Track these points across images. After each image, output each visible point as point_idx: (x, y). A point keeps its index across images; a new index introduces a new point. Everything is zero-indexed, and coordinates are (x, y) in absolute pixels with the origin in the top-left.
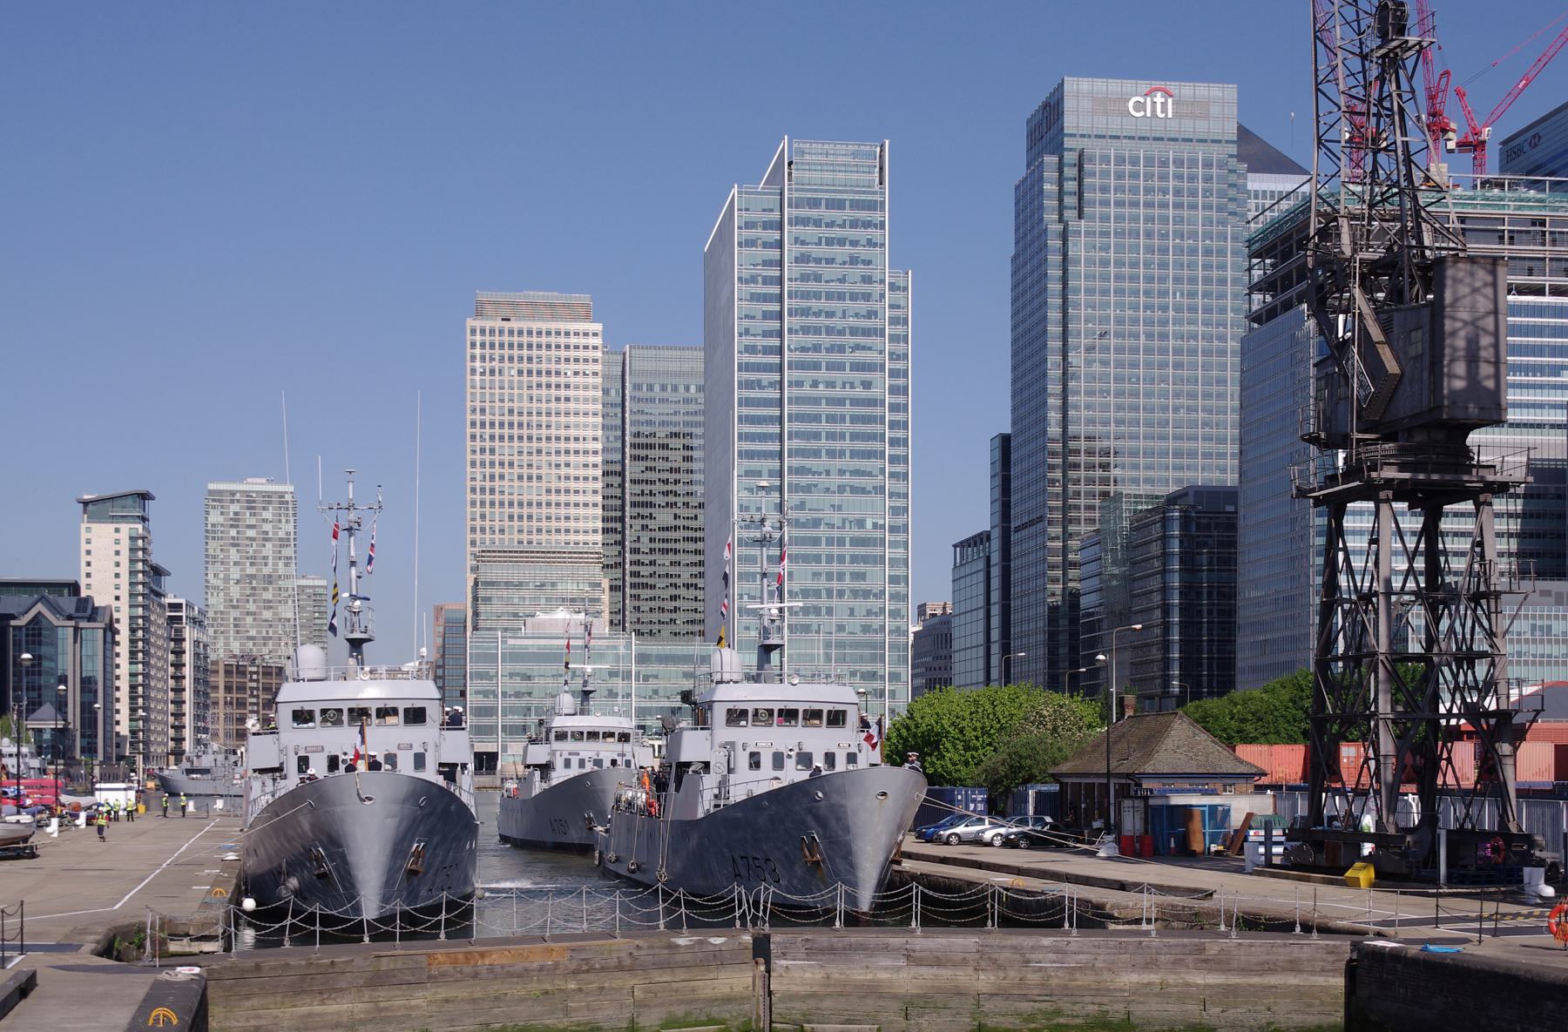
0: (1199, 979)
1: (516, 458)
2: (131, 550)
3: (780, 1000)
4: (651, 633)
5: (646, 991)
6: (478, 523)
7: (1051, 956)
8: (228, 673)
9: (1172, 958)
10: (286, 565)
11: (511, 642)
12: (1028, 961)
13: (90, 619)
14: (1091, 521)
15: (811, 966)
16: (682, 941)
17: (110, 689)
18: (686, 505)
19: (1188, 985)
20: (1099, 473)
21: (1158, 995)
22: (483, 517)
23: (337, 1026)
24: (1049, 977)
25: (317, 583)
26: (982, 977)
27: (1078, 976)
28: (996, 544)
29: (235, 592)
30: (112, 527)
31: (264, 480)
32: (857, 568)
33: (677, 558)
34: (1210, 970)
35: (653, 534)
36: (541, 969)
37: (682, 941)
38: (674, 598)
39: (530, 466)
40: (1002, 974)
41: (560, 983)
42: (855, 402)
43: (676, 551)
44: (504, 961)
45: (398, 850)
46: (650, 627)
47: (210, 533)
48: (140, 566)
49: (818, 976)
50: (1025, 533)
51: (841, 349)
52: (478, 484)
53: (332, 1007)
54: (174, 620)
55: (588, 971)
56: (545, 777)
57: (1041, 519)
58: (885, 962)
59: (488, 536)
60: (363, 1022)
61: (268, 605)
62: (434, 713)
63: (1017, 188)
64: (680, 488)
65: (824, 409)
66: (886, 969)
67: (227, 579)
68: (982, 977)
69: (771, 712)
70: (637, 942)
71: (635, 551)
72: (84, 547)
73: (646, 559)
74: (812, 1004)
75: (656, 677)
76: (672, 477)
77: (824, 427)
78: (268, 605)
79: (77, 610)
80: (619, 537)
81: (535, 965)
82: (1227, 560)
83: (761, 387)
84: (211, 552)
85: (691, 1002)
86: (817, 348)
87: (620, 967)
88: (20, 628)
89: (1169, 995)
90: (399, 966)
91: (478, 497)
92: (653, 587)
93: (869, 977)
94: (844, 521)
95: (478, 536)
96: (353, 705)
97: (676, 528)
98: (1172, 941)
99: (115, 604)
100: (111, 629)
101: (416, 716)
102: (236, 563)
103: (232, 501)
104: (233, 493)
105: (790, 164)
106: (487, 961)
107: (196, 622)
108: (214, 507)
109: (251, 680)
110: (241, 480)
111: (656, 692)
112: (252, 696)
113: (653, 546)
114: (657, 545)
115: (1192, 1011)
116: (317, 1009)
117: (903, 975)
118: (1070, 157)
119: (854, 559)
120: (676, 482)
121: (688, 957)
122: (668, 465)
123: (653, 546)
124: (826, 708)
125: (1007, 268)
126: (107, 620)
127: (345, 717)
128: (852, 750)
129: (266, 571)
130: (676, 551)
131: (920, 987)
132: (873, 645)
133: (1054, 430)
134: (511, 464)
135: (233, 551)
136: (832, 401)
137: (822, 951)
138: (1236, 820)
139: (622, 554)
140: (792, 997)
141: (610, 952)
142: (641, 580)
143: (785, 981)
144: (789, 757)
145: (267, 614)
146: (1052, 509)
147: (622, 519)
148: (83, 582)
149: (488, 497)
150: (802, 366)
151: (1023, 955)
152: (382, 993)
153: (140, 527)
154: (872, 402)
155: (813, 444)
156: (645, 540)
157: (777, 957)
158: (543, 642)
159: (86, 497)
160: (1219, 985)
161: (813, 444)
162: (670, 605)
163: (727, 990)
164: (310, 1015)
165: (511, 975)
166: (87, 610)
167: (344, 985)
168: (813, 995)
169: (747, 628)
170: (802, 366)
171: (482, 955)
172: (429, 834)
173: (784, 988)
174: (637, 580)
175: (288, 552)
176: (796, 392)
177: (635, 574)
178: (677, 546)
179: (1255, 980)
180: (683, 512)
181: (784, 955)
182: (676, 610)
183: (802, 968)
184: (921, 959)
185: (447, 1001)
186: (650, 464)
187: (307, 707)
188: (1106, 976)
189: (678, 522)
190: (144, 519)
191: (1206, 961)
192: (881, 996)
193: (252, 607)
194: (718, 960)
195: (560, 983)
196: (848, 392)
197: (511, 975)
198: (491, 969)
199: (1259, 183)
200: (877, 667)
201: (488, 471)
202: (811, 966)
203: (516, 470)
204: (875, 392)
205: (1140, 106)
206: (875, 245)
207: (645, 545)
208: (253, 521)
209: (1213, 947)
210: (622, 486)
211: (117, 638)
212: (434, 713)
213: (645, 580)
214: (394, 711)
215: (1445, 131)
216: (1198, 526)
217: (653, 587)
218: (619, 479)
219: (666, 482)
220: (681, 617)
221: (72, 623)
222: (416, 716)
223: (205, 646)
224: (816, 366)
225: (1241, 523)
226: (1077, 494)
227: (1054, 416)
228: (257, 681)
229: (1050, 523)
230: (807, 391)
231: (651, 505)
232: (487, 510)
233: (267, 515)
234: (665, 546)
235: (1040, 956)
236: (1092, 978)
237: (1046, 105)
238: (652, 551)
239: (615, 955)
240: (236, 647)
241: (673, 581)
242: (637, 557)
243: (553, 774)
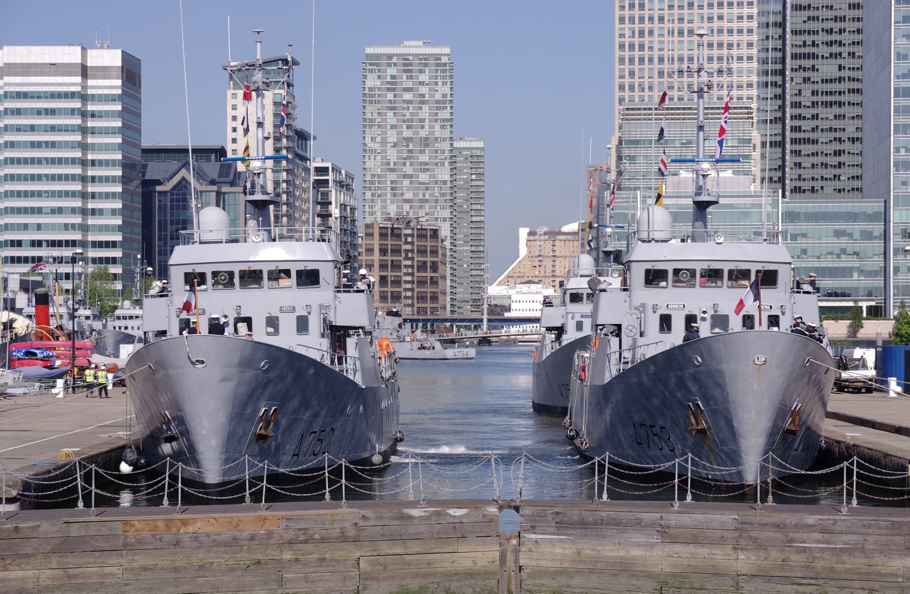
1: (666, 12)
3: (530, 576)
4: (813, 190)
5: (373, 564)
6: (627, 80)
7: (817, 536)
8: (383, 235)
10: (443, 127)
12: (791, 541)
13: (232, 184)
18: (852, 55)
22: (632, 74)
26: (741, 557)
27: (845, 557)
29: (392, 155)
31: (420, 43)
33: (841, 111)
35: (815, 87)
36: (252, 538)
38: (838, 153)
39: (681, 20)
40: (762, 554)
41: (273, 553)
43: (840, 104)
44: (209, 529)
45: (241, 411)
46: (812, 183)
47: (369, 97)
48: (283, 129)
52: (627, 41)
54: (320, 184)
55: (306, 542)
56: (558, 338)
58: (637, 537)
59: (637, 93)
61: (424, 167)
62: (328, 275)
64: (846, 38)
66: (639, 545)
67: (384, 142)
68: (741, 557)
69: (693, 272)
70: (363, 512)
71: (796, 105)
73: (808, 113)
74: (562, 580)
75: (804, 236)
76: (836, 26)
78: (424, 167)
79: (221, 175)
80: (779, 91)
81: (245, 534)
84: (368, 116)
85: (427, 575)
87: (343, 538)
88: (165, 193)
91: (627, 54)
92: (815, 142)
93: (622, 553)
95: (627, 93)
96: (245, 267)
97: (840, 80)
101: (309, 278)
102: (393, 127)
103: (389, 65)
104: (390, 57)
106: (190, 529)
107: (342, 185)
108: (371, 71)
109: (406, 243)
110: (398, 44)
111: (804, 251)
112: (407, 258)
113: (815, 99)
114: (819, 98)
120: (841, 31)
122: (830, 14)
123: (815, 99)
124: (754, 268)
127: (237, 280)
128: (774, 312)
129: (423, 133)
130: (840, 104)
134: (661, 19)
135: (390, 114)
137: (572, 525)
139: (782, 108)
140: (541, 573)
141: (333, 521)
142: (802, 135)
144: (704, 319)
145: (423, 177)
147: (782, 72)
148: (229, 147)
149: (637, 54)
152: (72, 560)
153: (283, 92)
156: (807, 93)
162: (834, 160)
167: (29, 551)
168: (563, 572)
172: (282, 400)
173: (534, 563)
174: (798, 135)
175: (445, 114)
177: (795, 129)
178: (842, 98)
180: (848, 62)
182: (840, 165)
183: (551, 542)
185: (145, 569)
186: (812, 13)
187: (199, 269)
188: (878, 559)
189: (843, 74)
192: (634, 575)
193: (408, 170)
197: (217, 544)
198: (195, 537)
201: (637, 26)
202: (562, 541)
203: (667, 25)
207: (807, 98)
208: (409, 84)
210: (783, 37)
212: (328, 275)
213: (806, 135)
214: (287, 273)
217: (815, 142)
218: (779, 31)
219: (830, 31)
220: (845, 173)
221: (215, 188)
222: (309, 278)
223: (353, 209)
228: (412, 243)
231: (814, 56)
232: (636, 67)
233: (423, 78)
234: (829, 98)
236: (863, 561)
238: (814, 104)
239: (337, 525)
240: (392, 210)
241: (838, 135)
242: (797, 111)
243: (564, 337)
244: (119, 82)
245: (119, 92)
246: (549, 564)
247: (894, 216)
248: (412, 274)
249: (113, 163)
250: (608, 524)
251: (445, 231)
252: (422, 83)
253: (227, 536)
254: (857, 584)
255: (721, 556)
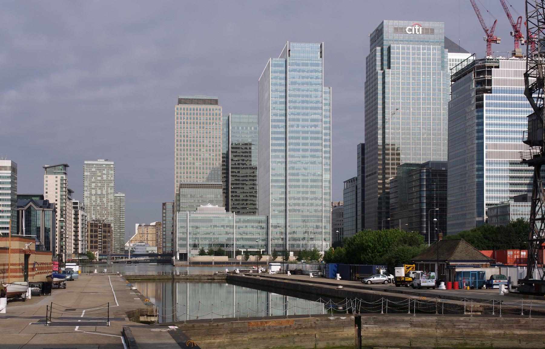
0: (518, 332)
2: (61, 184)
5: (320, 335)
7: (464, 324)
9: (508, 324)
11: (192, 215)
12: (455, 326)
14: (393, 173)
15: (376, 327)
16: (331, 318)
17: (54, 231)
19: (514, 334)
20: (396, 157)
21: (503, 338)
23: (219, 347)
24: (463, 331)
25: (121, 195)
26: (438, 331)
27: (473, 331)
28: (360, 181)
30: (55, 176)
32: (312, 190)
34: (522, 329)
36: (286, 327)
37: (331, 318)
40: (445, 330)
41: (291, 333)
42: (312, 132)
48: (64, 189)
49: (378, 331)
50: (369, 178)
51: (307, 114)
53: (218, 341)
55: (301, 329)
57: (375, 173)
58: (402, 326)
60: (227, 346)
63: (367, 58)
65: (301, 135)
66: (403, 328)
68: (438, 331)
72: (45, 183)
77: (301, 141)
79: (43, 204)
81: (284, 326)
82: (443, 187)
83: (279, 128)
86: (298, 114)
87: (311, 327)
89: (507, 338)
90: (239, 326)
93: (397, 331)
94: (308, 173)
98: (508, 319)
99: (56, 202)
100: (55, 211)
105: (289, 51)
106: (268, 325)
107: (82, 209)
115: (516, 343)
116: (213, 341)
117: (409, 330)
118: (385, 48)
119: (312, 187)
121: (334, 323)
125: (363, 86)
126: (53, 207)
131: (416, 335)
132: (318, 217)
133: (380, 142)
136: (304, 132)
137: (380, 322)
138: (487, 277)
141: (308, 322)
143: (366, 332)
146: (379, 169)
148: (45, 195)
149: (182, 166)
150: (294, 120)
151: (453, 323)
152: (234, 335)
153: (64, 176)
154: (317, 133)
155: (297, 147)
157: (364, 324)
158: (204, 215)
159: (46, 166)
160: (525, 334)
161: (297, 147)
163: (346, 335)
164: (210, 343)
165: (275, 330)
166: (46, 205)
167: (221, 333)
169: (274, 211)
170: (294, 120)
171: (266, 322)
173: (366, 335)
176: (292, 129)
179: (539, 333)
181: (366, 323)
183: (372, 328)
184: (416, 325)
185: (255, 338)
188: (484, 331)
190: (65, 174)
191: (520, 326)
192: (401, 338)
194: (344, 325)
195: (291, 333)
196: (310, 129)
197: (275, 330)
199: (452, 56)
200: (320, 224)
202: (376, 327)
204: (319, 129)
205: (410, 30)
206: (319, 78)
209: (523, 321)
211: (57, 214)
215: (520, 37)
216: (432, 174)
221: (42, 209)
224: (298, 120)
225: (449, 174)
226: (388, 164)
227: (380, 137)
229: (379, 174)
230: (295, 129)
231: (238, 168)
235: (460, 324)
237: (377, 30)
239: (310, 323)
244: (10, 172)
245: (10, 175)
246: (371, 335)
247: (271, 221)
248: (101, 239)
249: (8, 200)
250: (392, 321)
251: (112, 225)
252: (104, 174)
253: (278, 327)
254: (477, 339)
255: (431, 331)
